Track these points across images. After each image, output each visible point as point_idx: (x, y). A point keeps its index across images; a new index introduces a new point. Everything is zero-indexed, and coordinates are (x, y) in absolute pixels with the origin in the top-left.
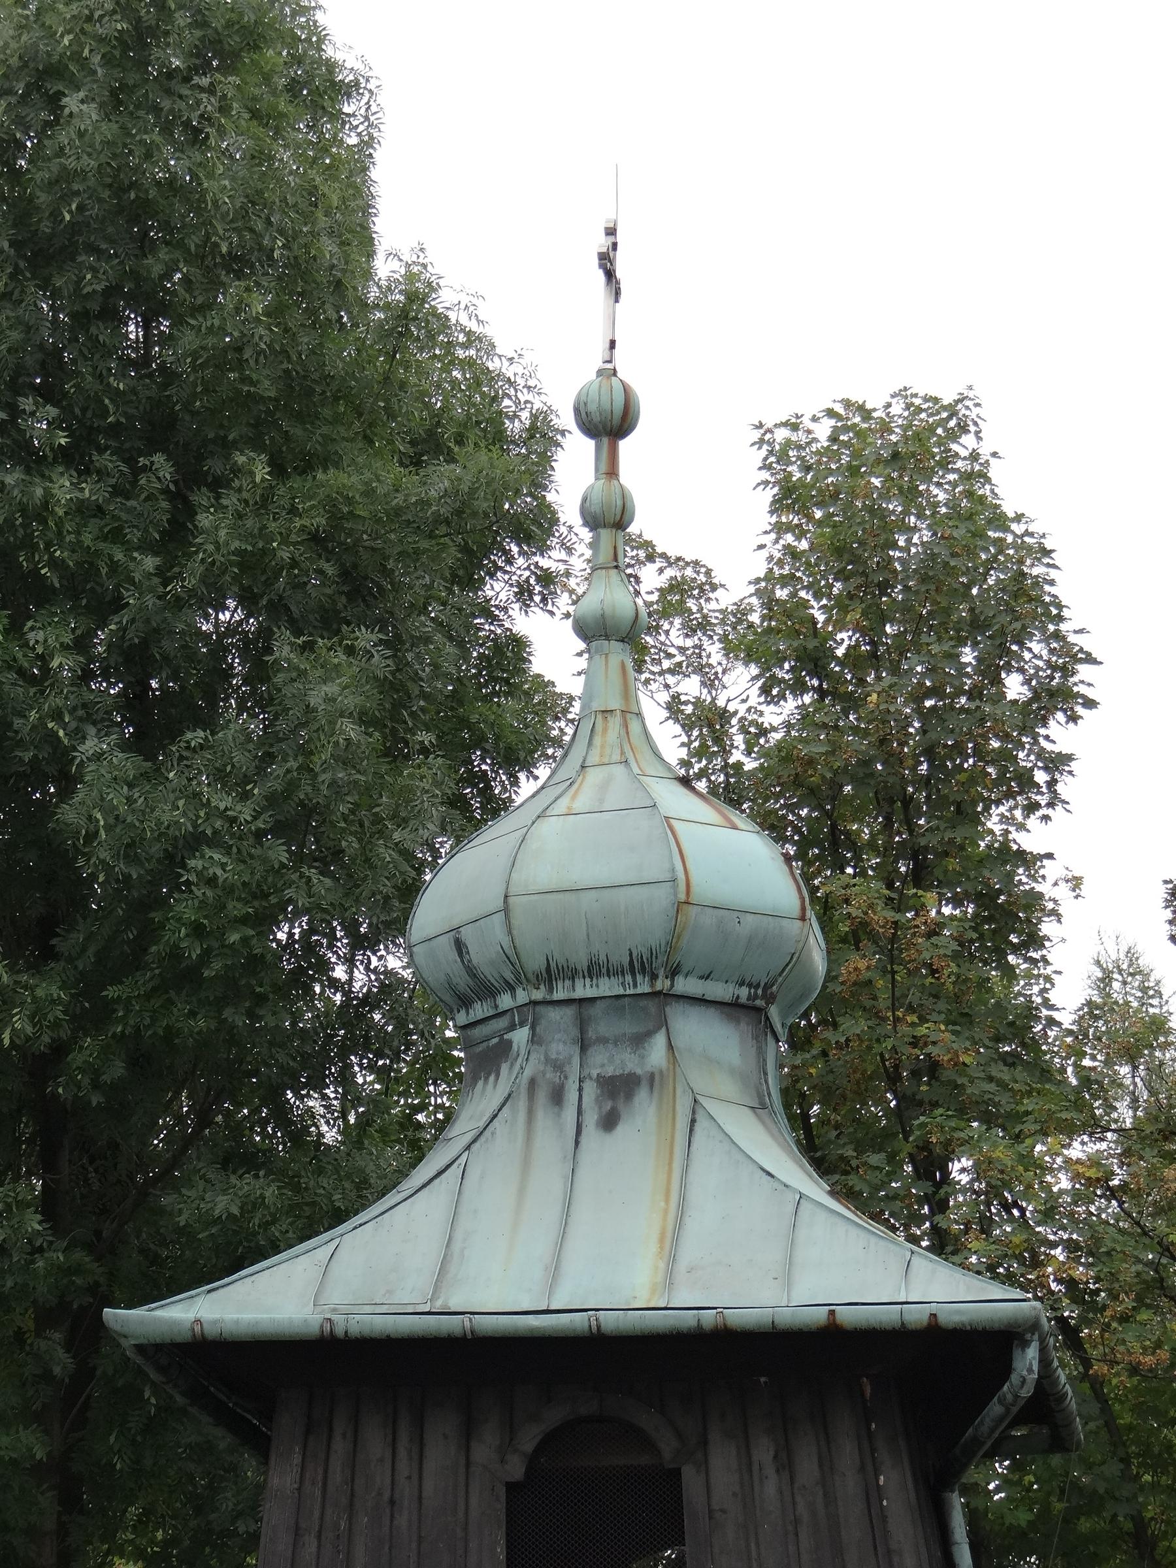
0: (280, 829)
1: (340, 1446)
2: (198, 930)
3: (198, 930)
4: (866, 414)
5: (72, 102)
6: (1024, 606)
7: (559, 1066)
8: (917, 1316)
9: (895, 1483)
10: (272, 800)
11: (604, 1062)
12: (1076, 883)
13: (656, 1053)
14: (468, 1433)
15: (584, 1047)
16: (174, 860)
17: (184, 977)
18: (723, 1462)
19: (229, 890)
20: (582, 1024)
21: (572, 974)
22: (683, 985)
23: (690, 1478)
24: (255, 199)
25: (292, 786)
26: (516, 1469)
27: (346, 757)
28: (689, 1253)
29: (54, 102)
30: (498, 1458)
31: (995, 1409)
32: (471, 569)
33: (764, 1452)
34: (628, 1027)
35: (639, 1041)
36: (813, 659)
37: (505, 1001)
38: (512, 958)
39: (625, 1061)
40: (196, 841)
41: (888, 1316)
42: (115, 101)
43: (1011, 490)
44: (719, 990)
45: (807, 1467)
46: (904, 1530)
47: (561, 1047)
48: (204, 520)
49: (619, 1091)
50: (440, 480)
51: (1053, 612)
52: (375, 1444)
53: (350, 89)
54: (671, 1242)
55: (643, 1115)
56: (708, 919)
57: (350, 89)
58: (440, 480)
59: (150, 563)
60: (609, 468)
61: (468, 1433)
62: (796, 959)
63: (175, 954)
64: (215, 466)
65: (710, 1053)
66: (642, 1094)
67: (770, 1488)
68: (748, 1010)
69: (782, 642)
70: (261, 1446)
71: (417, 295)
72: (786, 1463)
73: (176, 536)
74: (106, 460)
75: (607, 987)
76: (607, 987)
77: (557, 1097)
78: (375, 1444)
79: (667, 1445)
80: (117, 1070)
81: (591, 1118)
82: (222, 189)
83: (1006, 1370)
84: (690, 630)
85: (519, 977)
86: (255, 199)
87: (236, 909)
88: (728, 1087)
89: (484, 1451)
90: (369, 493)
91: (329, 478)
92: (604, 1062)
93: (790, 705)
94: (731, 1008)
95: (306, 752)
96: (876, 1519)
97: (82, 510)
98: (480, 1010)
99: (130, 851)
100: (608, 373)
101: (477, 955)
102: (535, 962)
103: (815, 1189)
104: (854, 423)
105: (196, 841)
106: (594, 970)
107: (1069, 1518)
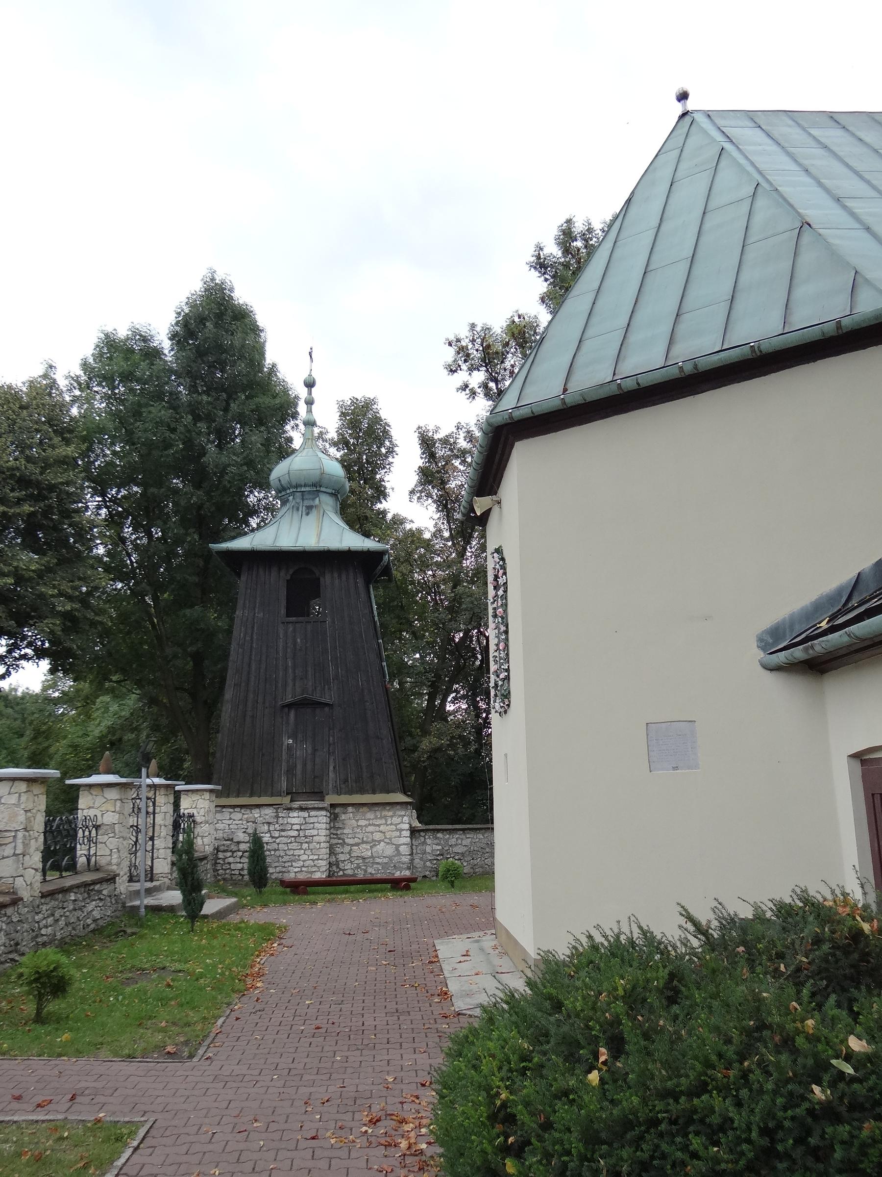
0: (245, 464)
1: (254, 573)
2: (229, 482)
3: (229, 482)
4: (357, 400)
5: (208, 324)
6: (386, 434)
7: (298, 504)
8: (365, 549)
9: (360, 581)
10: (244, 458)
11: (307, 503)
12: (393, 489)
13: (317, 501)
14: (280, 569)
15: (303, 500)
16: (225, 468)
17: (227, 491)
18: (328, 577)
19: (235, 474)
20: (303, 496)
21: (301, 486)
22: (322, 489)
23: (322, 579)
24: (243, 346)
25: (248, 455)
26: (289, 577)
27: (258, 450)
28: (322, 537)
29: (204, 325)
30: (286, 575)
31: (379, 567)
32: (283, 421)
33: (336, 575)
34: (311, 496)
35: (313, 499)
36: (346, 443)
37: (288, 491)
38: (290, 483)
39: (310, 503)
40: (229, 465)
41: (360, 549)
42: (216, 325)
43: (383, 415)
44: (329, 491)
45: (344, 577)
46: (363, 595)
47: (298, 500)
48: (232, 405)
49: (309, 509)
50: (277, 401)
51: (390, 438)
52: (261, 572)
53: (262, 331)
54: (319, 536)
55: (314, 513)
56: (327, 476)
57: (262, 331)
58: (277, 401)
59: (221, 413)
60: (310, 393)
61: (280, 569)
62: (343, 486)
63: (225, 486)
64: (234, 396)
65: (327, 503)
66: (314, 509)
67: (337, 581)
68: (334, 495)
69: (342, 442)
70: (239, 575)
71: (273, 369)
72: (340, 577)
73: (226, 409)
74: (214, 394)
75: (308, 489)
76: (308, 489)
77: (298, 509)
78: (261, 572)
79: (317, 573)
80: (213, 509)
81: (304, 513)
82: (237, 343)
83: (382, 559)
84: (323, 441)
85: (291, 486)
86: (243, 346)
87: (236, 478)
88: (330, 508)
89: (282, 573)
90: (264, 403)
91: (257, 400)
92: (307, 503)
93: (342, 452)
94: (331, 494)
95: (251, 449)
96: (356, 587)
97: (209, 403)
98: (283, 493)
99: (216, 466)
100: (310, 375)
101: (283, 482)
102: (294, 484)
103: (347, 527)
104: (354, 401)
105: (229, 465)
106: (305, 486)
107: (389, 602)
